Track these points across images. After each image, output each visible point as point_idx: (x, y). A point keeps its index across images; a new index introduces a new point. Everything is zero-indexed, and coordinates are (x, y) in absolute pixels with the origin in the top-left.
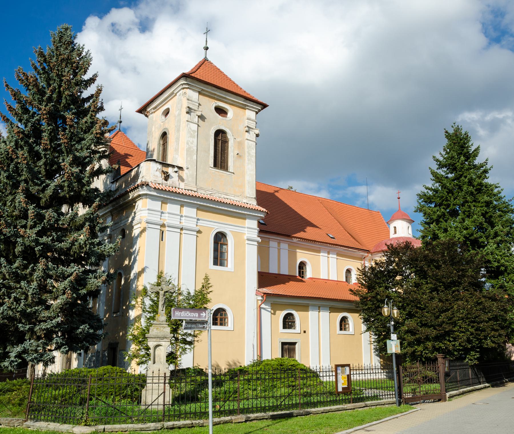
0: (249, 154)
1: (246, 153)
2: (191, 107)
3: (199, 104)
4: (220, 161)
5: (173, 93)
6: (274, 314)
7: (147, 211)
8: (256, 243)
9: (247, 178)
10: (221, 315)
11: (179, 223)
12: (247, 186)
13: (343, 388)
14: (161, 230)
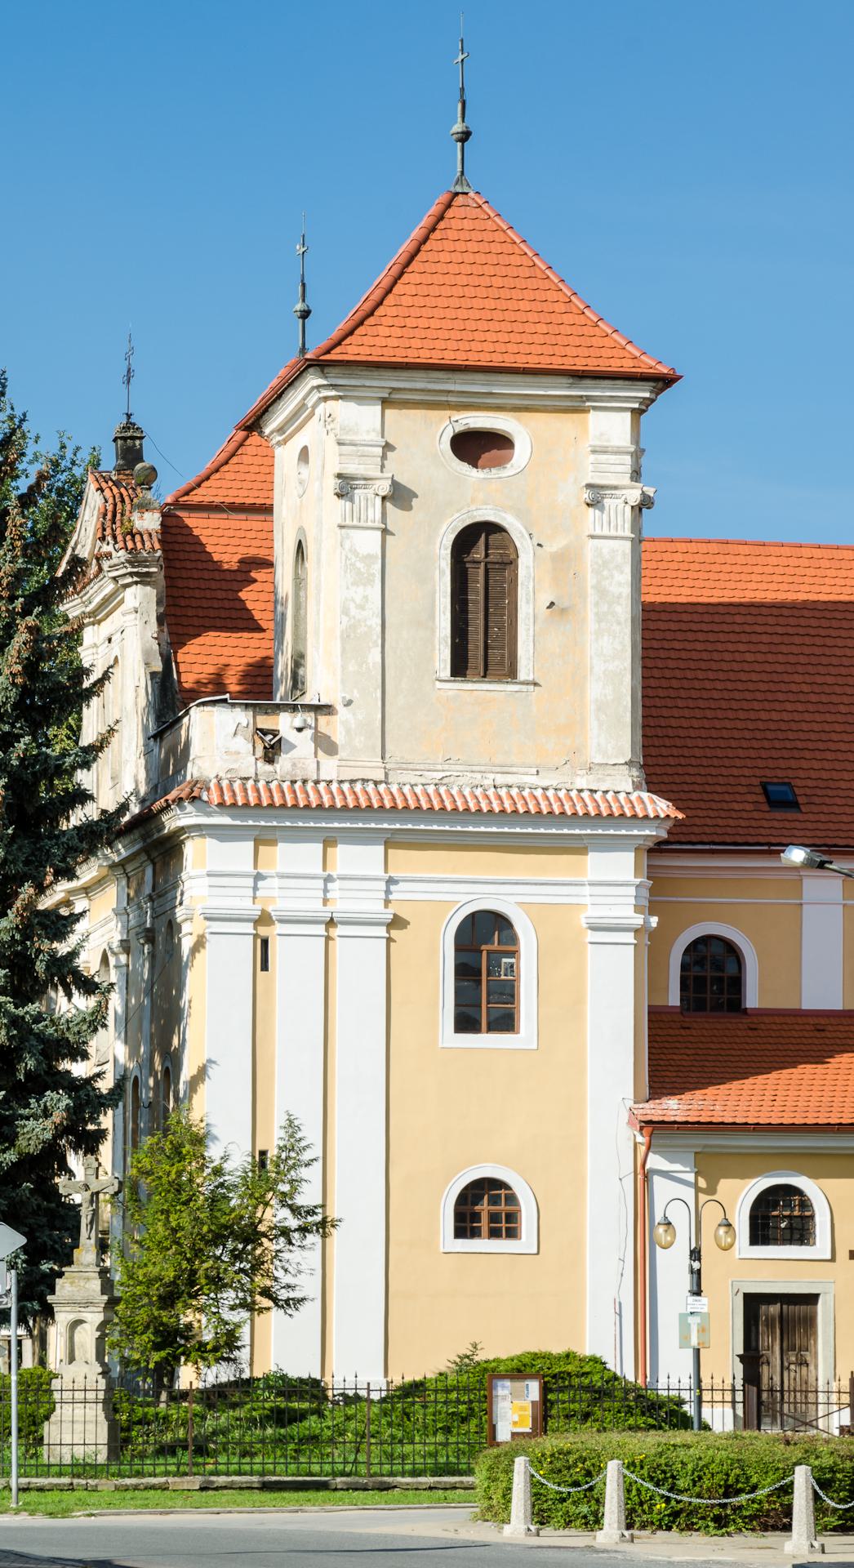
0: (602, 593)
1: (590, 591)
2: (350, 469)
3: (388, 447)
4: (480, 636)
5: (302, 407)
6: (711, 1190)
7: (207, 881)
8: (630, 937)
9: (595, 690)
10: (494, 1200)
11: (319, 905)
12: (592, 724)
13: (514, 1435)
14: (256, 936)
